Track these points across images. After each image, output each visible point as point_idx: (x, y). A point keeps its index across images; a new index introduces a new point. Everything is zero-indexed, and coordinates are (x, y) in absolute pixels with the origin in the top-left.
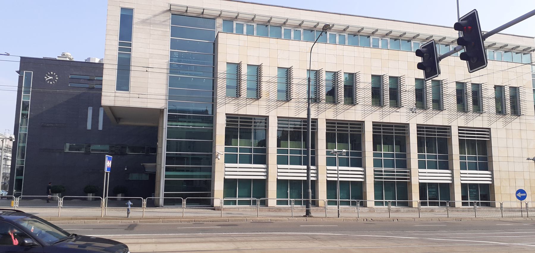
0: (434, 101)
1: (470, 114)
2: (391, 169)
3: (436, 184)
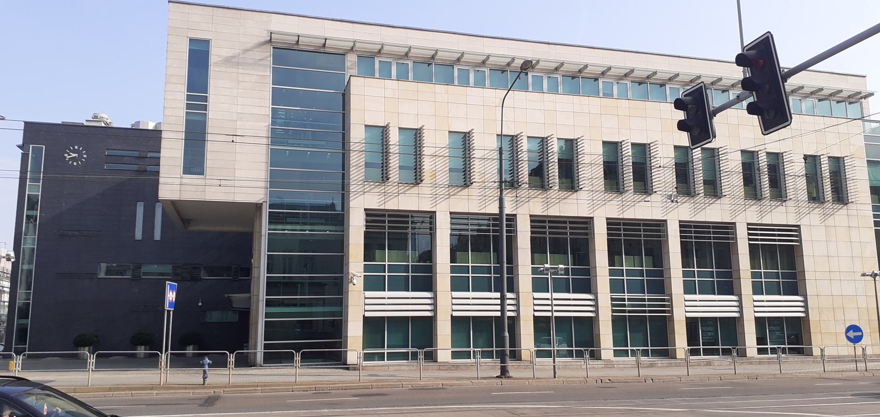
0: (705, 182)
1: (766, 202)
3: (715, 319)
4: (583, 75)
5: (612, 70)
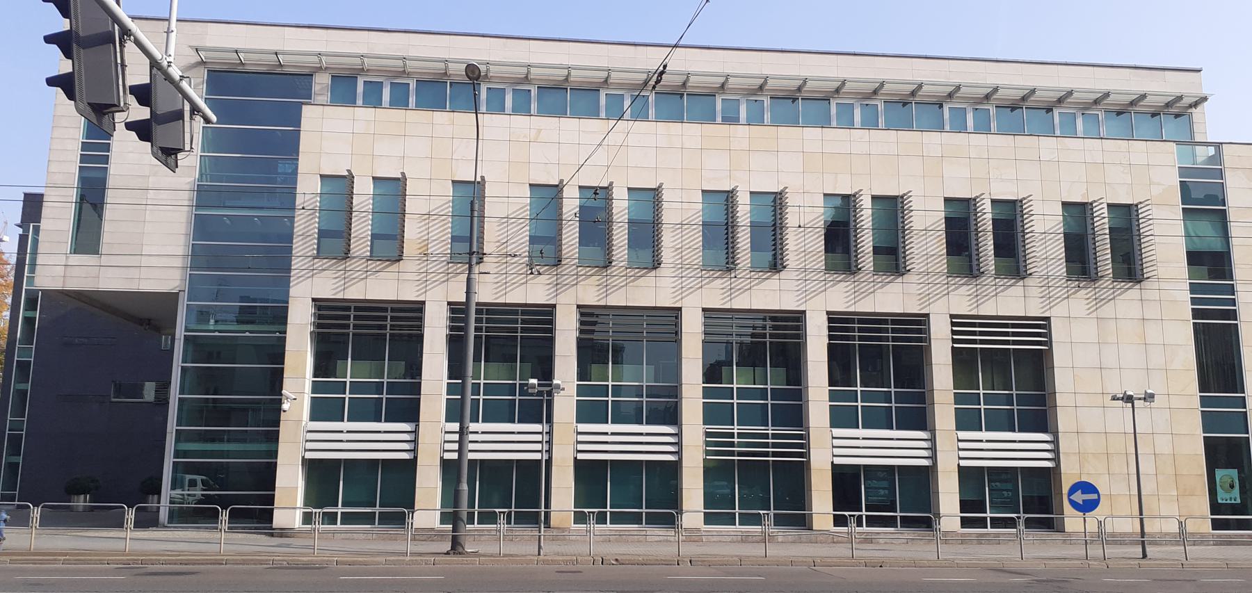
0: (877, 250)
1: (987, 280)
2: (759, 429)
3: (890, 469)
4: (1028, 104)
5: (1149, 98)
